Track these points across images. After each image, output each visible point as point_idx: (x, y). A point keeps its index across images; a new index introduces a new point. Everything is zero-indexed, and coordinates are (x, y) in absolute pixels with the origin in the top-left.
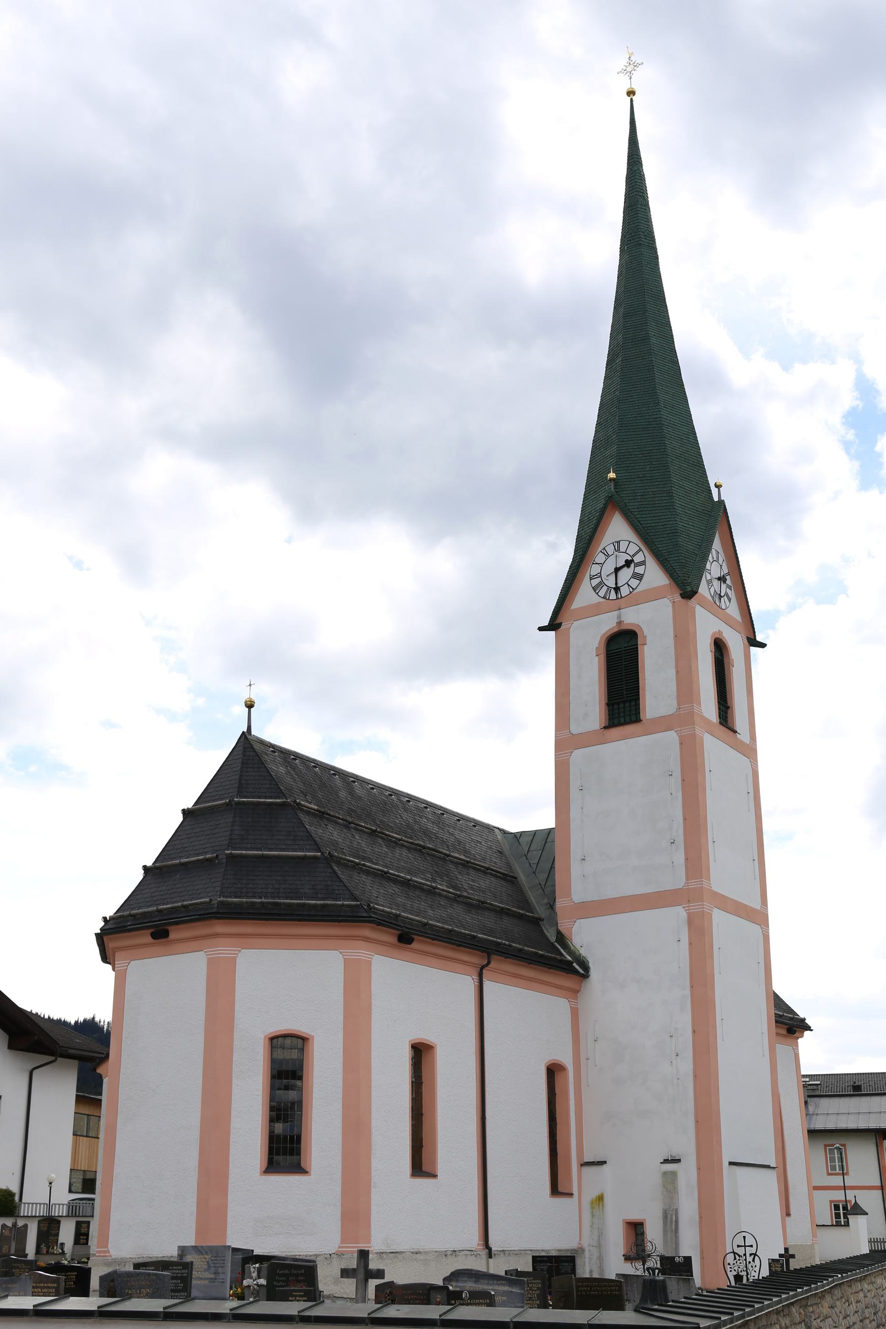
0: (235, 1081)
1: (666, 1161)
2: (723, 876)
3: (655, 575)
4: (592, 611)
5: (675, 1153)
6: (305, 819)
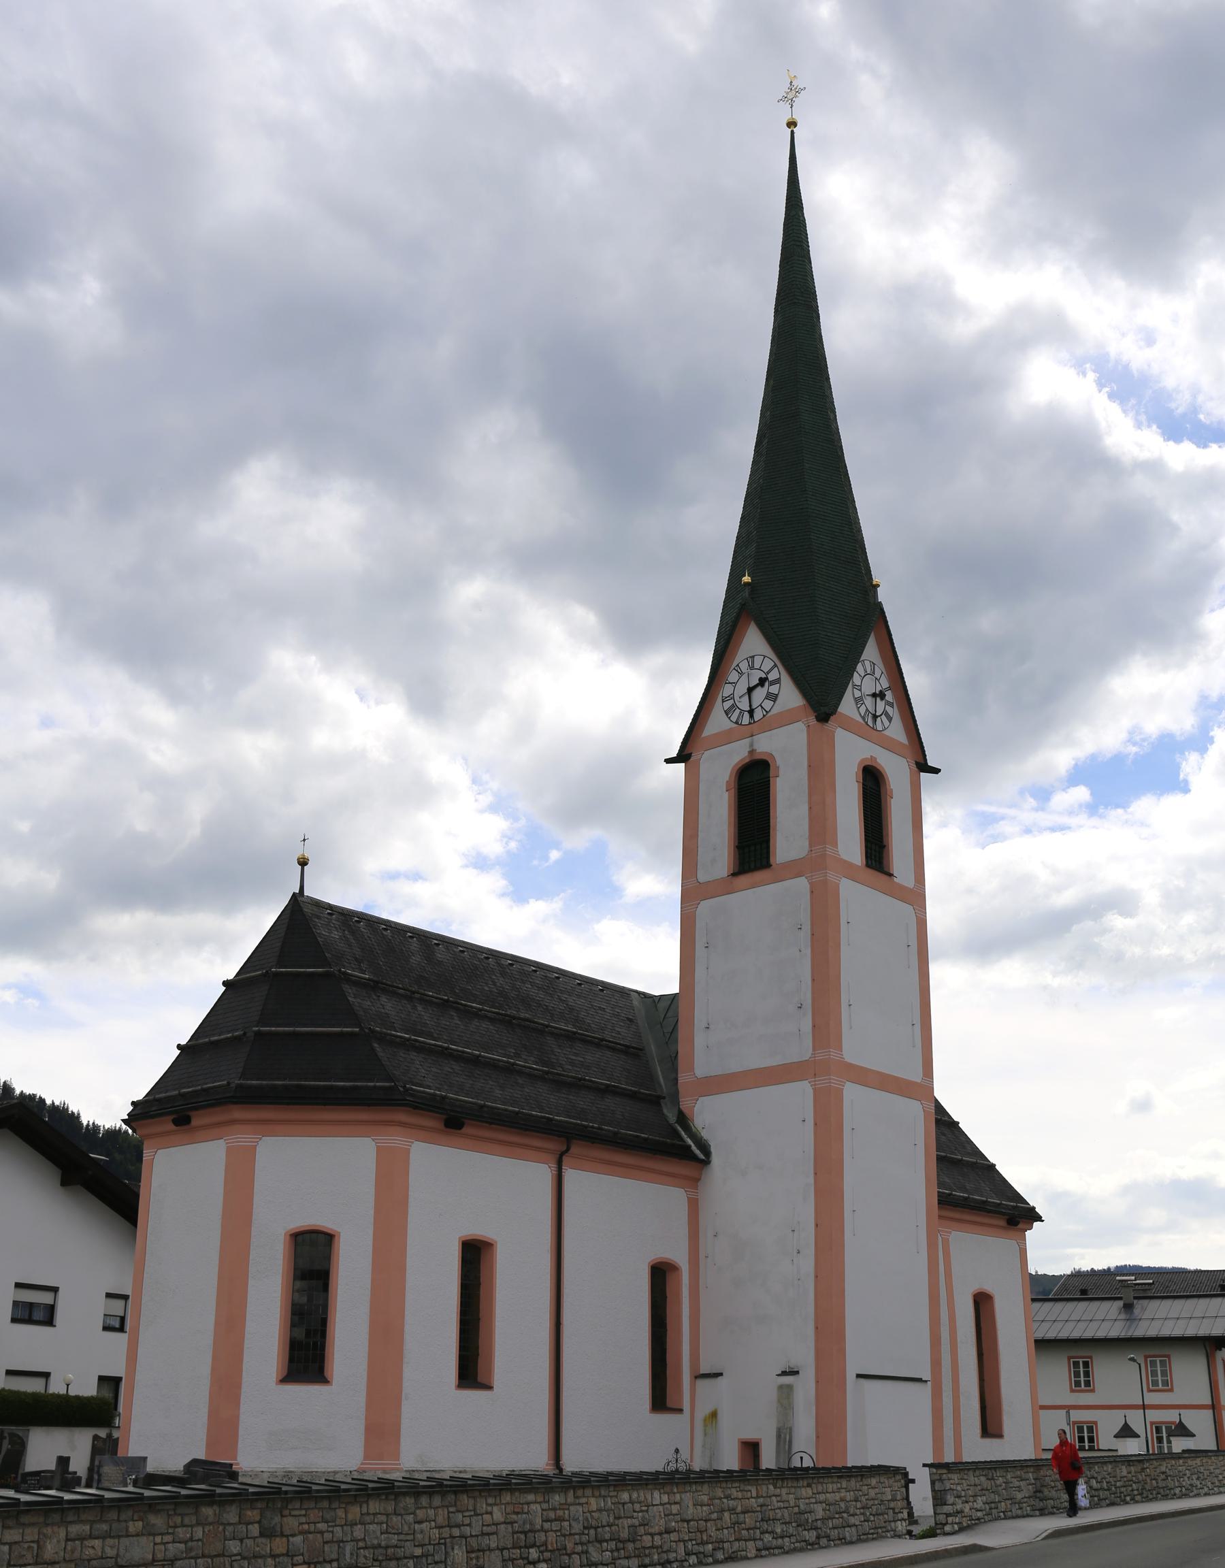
0: (251, 1282)
1: (784, 1373)
2: (862, 1043)
3: (790, 696)
4: (726, 738)
5: (794, 1363)
6: (349, 990)
